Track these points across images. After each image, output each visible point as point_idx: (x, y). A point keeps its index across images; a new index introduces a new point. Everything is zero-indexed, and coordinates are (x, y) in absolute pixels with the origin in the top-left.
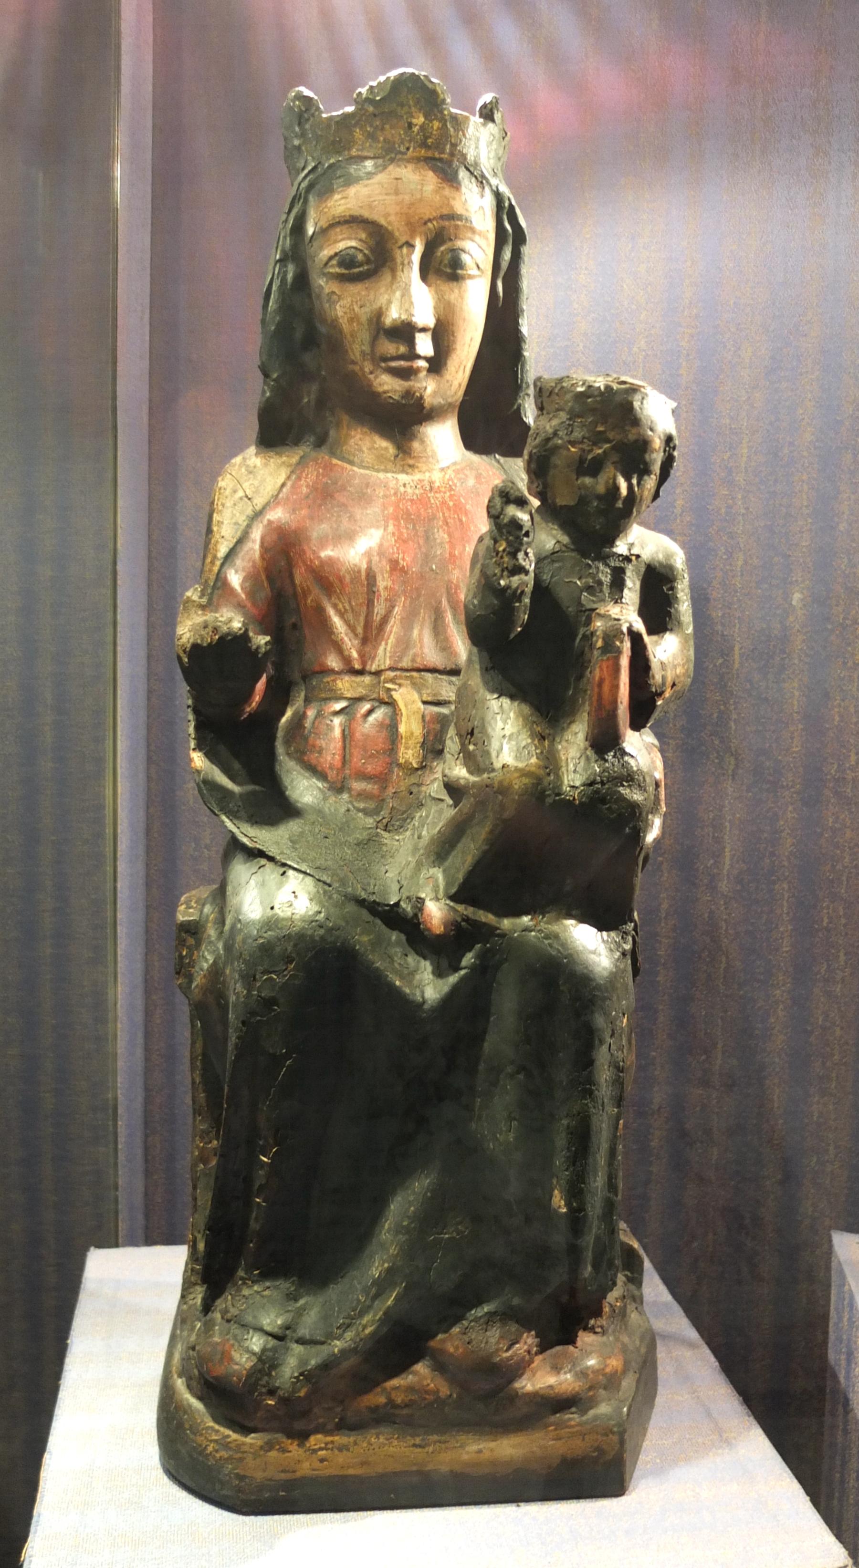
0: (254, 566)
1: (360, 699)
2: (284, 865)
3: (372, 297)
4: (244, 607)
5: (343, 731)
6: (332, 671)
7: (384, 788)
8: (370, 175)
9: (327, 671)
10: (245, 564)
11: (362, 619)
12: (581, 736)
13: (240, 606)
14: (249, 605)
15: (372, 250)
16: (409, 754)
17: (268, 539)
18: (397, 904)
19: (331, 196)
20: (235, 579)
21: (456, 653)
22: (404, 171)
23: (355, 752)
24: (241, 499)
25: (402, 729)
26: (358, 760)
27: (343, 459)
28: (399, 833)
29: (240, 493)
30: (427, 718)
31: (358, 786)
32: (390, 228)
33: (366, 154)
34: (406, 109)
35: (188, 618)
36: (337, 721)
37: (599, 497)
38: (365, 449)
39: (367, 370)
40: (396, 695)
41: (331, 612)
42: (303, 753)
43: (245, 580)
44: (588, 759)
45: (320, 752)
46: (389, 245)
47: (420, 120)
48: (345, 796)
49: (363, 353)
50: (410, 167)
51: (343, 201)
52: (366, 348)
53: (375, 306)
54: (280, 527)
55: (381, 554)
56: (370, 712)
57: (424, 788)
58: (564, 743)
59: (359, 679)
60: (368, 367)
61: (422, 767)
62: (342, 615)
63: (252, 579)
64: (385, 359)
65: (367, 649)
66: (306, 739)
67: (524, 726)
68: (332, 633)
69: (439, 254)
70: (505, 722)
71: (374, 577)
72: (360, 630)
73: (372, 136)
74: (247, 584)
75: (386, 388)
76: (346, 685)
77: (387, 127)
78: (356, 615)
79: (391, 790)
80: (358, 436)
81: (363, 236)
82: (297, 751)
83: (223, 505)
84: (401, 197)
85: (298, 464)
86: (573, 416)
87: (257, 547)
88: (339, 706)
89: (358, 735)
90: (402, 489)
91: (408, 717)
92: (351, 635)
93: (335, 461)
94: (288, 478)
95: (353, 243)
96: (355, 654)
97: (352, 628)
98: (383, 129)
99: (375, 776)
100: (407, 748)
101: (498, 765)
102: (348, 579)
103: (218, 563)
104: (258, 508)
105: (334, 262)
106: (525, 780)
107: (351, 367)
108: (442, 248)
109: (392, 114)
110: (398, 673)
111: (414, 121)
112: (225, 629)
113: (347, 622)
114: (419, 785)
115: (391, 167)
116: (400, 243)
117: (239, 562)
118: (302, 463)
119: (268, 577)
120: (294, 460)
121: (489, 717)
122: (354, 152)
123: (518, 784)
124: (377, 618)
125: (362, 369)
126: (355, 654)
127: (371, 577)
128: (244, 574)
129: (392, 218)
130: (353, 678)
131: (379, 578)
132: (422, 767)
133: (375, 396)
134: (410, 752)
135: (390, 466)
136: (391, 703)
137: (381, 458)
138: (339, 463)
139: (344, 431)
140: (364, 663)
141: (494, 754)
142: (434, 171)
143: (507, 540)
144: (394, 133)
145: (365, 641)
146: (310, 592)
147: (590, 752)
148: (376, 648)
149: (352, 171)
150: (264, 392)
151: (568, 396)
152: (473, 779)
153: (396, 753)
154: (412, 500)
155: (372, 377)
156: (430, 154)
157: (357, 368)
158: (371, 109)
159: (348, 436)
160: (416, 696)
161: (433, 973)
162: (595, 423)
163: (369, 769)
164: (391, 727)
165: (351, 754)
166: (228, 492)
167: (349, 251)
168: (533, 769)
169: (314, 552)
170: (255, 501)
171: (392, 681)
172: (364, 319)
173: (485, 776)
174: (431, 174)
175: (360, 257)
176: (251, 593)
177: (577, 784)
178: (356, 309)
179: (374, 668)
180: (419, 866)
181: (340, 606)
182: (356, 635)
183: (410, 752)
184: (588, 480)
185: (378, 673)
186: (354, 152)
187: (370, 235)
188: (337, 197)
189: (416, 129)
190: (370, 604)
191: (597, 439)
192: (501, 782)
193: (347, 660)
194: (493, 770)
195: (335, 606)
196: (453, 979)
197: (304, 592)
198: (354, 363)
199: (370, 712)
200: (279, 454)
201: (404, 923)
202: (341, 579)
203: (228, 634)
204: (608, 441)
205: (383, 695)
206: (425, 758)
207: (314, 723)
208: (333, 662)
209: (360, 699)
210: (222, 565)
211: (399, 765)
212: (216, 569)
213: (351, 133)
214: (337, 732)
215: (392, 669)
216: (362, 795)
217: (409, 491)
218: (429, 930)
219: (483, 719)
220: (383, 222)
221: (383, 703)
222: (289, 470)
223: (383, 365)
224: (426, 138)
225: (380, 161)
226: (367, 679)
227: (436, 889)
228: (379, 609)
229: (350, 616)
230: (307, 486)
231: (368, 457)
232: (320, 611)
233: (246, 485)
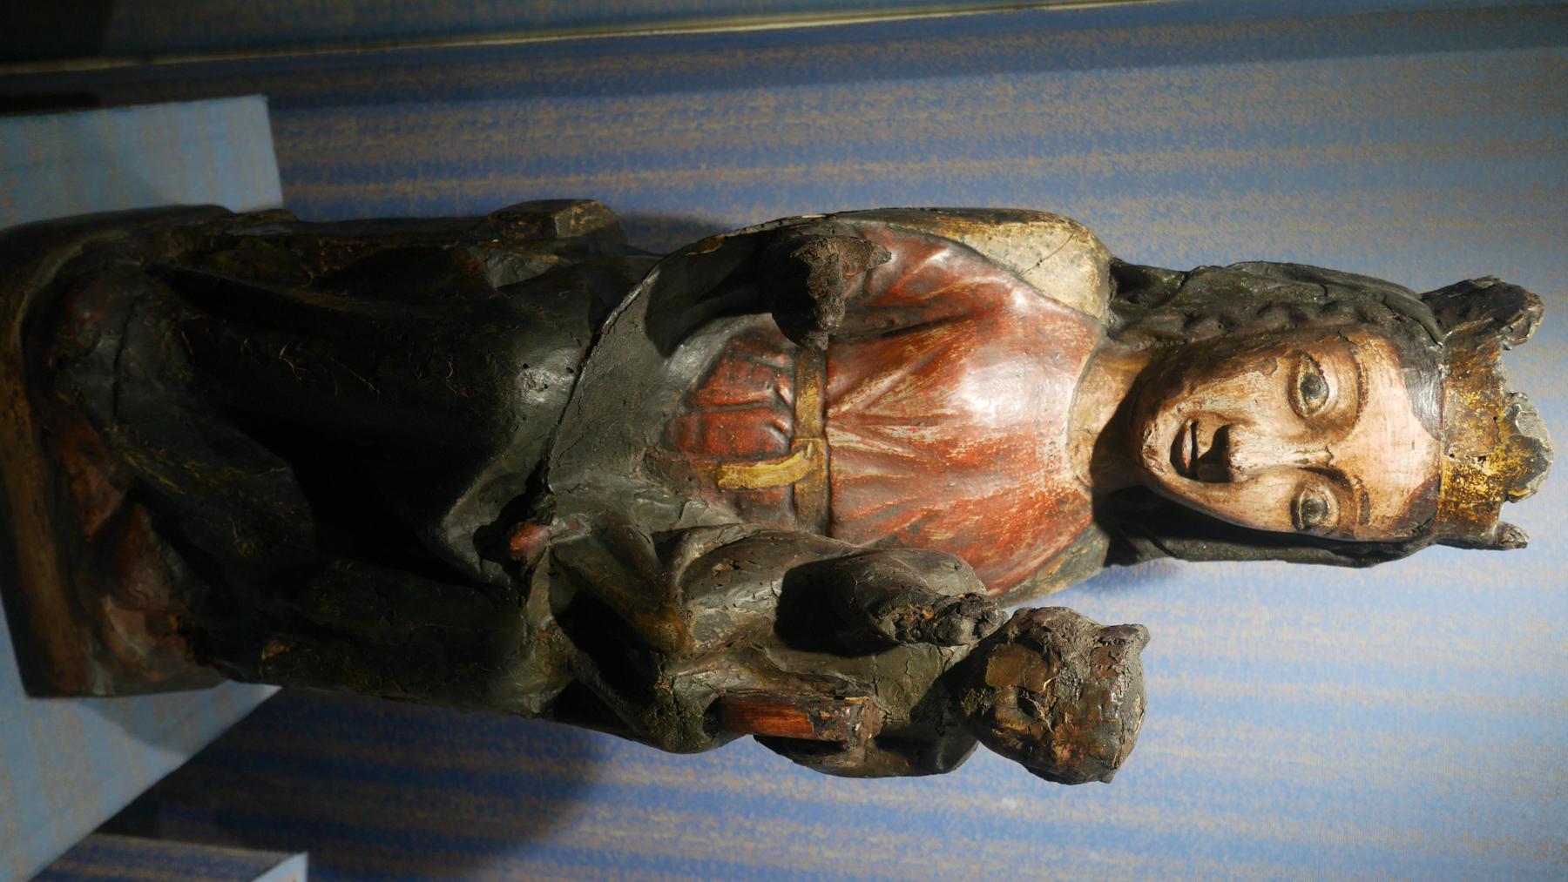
0: (954, 279)
1: (795, 418)
2: (580, 370)
3: (1268, 412)
4: (904, 273)
5: (753, 402)
6: (827, 383)
7: (692, 450)
8: (1419, 413)
9: (828, 374)
10: (956, 269)
11: (887, 413)
12: (735, 682)
13: (905, 268)
14: (906, 278)
15: (1323, 416)
16: (733, 475)
17: (988, 292)
18: (548, 491)
19: (1395, 365)
20: (939, 258)
21: (747, 628)
22: (1424, 451)
23: (732, 417)
24: (1039, 254)
25: (760, 466)
26: (722, 421)
27: (1089, 367)
28: (642, 470)
29: (1045, 253)
30: (775, 491)
31: (694, 421)
32: (1350, 437)
33: (1446, 407)
34: (1502, 455)
35: (849, 251)
36: (769, 392)
37: (992, 710)
38: (1098, 394)
39: (1183, 405)
40: (798, 456)
41: (896, 376)
42: (731, 357)
43: (937, 269)
44: (706, 695)
45: (732, 378)
46: (1330, 435)
47: (1488, 469)
48: (682, 410)
49: (1202, 402)
50: (1429, 459)
51: (1386, 380)
52: (1207, 406)
53: (1257, 418)
54: (1002, 304)
55: (964, 428)
56: (780, 429)
57: (696, 492)
58: (726, 665)
59: (818, 414)
60: (1187, 407)
61: (719, 489)
62: (892, 389)
63: (939, 277)
64: (1194, 427)
65: (853, 420)
66: (748, 359)
67: (741, 628)
68: (871, 378)
69: (1321, 488)
70: (742, 607)
71: (936, 424)
72: (874, 411)
73: (1469, 414)
74: (932, 273)
75: (1161, 427)
76: (811, 398)
77: (1480, 432)
78: (891, 407)
79: (691, 457)
80: (1114, 385)
81: (1342, 406)
82: (734, 349)
83: (1032, 233)
84: (1390, 448)
85: (1084, 314)
86: (1084, 687)
87: (978, 279)
88: (786, 393)
89: (751, 418)
90: (1048, 441)
91: (775, 471)
92: (868, 401)
93: (1085, 359)
94: (1066, 306)
95: (1333, 393)
96: (845, 408)
97: (875, 403)
98: (1478, 427)
99: (705, 441)
100: (739, 472)
101: (690, 605)
102: (933, 394)
103: (957, 238)
104: (1027, 277)
105: (1312, 370)
106: (674, 636)
107: (1187, 384)
108: (1328, 492)
109: (1497, 441)
110: (825, 457)
111: (1487, 464)
112: (825, 307)
113: (884, 395)
114: (699, 488)
115: (1428, 436)
116: (1332, 449)
117: (959, 262)
118: (1086, 319)
119: (942, 295)
120: (1090, 310)
121: (750, 587)
122: (1450, 392)
123: (669, 629)
124: (887, 430)
125: (1184, 399)
126: (845, 408)
127: (933, 421)
128: (944, 267)
129: (1362, 440)
130: (819, 407)
131: (934, 429)
132: (719, 489)
133: (1153, 413)
134: (735, 476)
135: (1077, 425)
136: (789, 453)
137: (1085, 414)
138: (1083, 364)
139: (1123, 367)
140: (835, 418)
141: (704, 599)
142: (1423, 485)
143: (933, 620)
144: (1473, 440)
145: (862, 417)
146: (920, 349)
147: (713, 696)
148: (854, 430)
149: (1426, 390)
150: (1168, 272)
151: (1106, 683)
152: (678, 575)
153: (734, 462)
154: (1034, 453)
155: (1175, 410)
156: (1445, 480)
157: (1185, 393)
158: (1503, 415)
159: (1114, 372)
160: (799, 477)
161: (481, 529)
162: (1073, 712)
163: (713, 434)
164: (764, 453)
165: (730, 413)
166: (1047, 237)
167: (1324, 388)
168: (688, 643)
169: (967, 351)
170: (1035, 272)
171: (815, 450)
172: (1241, 404)
173: (680, 591)
174: (1420, 481)
175: (1315, 402)
176: (921, 278)
177: (677, 686)
178: (1253, 396)
179: (829, 430)
180: (594, 506)
181: (902, 387)
182: (868, 407)
183: (735, 476)
184: (1012, 698)
185: (824, 435)
186: (1450, 392)
187: (1344, 414)
188: (1393, 372)
189: (1477, 466)
190: (904, 421)
191: (1056, 713)
192: (671, 610)
193: (838, 400)
194: (685, 600)
195: (903, 380)
196: (473, 557)
197: (922, 340)
198: (1193, 388)
199: (780, 429)
200: (1098, 290)
201: (526, 504)
202: (932, 386)
203: (819, 312)
204: (1054, 725)
205: (799, 441)
206: (730, 491)
207: (766, 366)
208: (838, 382)
209: (795, 418)
210: (955, 242)
211: (720, 465)
212: (950, 235)
213: (1474, 389)
214: (752, 395)
215: (830, 449)
216: (683, 427)
217: (1046, 449)
218: (514, 534)
219: (748, 580)
220: (1358, 429)
221: (791, 441)
222: (1076, 306)
223: (1190, 423)
224: (1465, 477)
225: (1436, 423)
226: (817, 423)
227: (562, 534)
228: (899, 431)
229: (890, 399)
230: (1054, 330)
231: (1087, 400)
232: (898, 362)
233: (1056, 258)
